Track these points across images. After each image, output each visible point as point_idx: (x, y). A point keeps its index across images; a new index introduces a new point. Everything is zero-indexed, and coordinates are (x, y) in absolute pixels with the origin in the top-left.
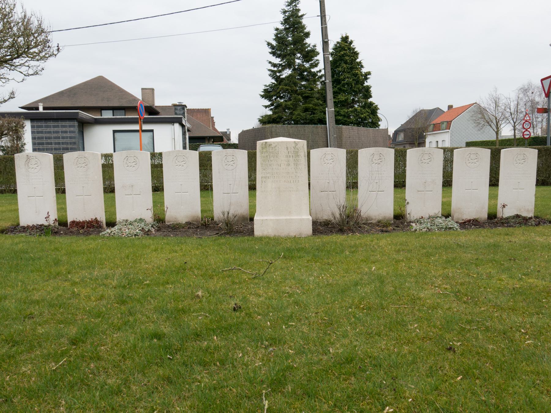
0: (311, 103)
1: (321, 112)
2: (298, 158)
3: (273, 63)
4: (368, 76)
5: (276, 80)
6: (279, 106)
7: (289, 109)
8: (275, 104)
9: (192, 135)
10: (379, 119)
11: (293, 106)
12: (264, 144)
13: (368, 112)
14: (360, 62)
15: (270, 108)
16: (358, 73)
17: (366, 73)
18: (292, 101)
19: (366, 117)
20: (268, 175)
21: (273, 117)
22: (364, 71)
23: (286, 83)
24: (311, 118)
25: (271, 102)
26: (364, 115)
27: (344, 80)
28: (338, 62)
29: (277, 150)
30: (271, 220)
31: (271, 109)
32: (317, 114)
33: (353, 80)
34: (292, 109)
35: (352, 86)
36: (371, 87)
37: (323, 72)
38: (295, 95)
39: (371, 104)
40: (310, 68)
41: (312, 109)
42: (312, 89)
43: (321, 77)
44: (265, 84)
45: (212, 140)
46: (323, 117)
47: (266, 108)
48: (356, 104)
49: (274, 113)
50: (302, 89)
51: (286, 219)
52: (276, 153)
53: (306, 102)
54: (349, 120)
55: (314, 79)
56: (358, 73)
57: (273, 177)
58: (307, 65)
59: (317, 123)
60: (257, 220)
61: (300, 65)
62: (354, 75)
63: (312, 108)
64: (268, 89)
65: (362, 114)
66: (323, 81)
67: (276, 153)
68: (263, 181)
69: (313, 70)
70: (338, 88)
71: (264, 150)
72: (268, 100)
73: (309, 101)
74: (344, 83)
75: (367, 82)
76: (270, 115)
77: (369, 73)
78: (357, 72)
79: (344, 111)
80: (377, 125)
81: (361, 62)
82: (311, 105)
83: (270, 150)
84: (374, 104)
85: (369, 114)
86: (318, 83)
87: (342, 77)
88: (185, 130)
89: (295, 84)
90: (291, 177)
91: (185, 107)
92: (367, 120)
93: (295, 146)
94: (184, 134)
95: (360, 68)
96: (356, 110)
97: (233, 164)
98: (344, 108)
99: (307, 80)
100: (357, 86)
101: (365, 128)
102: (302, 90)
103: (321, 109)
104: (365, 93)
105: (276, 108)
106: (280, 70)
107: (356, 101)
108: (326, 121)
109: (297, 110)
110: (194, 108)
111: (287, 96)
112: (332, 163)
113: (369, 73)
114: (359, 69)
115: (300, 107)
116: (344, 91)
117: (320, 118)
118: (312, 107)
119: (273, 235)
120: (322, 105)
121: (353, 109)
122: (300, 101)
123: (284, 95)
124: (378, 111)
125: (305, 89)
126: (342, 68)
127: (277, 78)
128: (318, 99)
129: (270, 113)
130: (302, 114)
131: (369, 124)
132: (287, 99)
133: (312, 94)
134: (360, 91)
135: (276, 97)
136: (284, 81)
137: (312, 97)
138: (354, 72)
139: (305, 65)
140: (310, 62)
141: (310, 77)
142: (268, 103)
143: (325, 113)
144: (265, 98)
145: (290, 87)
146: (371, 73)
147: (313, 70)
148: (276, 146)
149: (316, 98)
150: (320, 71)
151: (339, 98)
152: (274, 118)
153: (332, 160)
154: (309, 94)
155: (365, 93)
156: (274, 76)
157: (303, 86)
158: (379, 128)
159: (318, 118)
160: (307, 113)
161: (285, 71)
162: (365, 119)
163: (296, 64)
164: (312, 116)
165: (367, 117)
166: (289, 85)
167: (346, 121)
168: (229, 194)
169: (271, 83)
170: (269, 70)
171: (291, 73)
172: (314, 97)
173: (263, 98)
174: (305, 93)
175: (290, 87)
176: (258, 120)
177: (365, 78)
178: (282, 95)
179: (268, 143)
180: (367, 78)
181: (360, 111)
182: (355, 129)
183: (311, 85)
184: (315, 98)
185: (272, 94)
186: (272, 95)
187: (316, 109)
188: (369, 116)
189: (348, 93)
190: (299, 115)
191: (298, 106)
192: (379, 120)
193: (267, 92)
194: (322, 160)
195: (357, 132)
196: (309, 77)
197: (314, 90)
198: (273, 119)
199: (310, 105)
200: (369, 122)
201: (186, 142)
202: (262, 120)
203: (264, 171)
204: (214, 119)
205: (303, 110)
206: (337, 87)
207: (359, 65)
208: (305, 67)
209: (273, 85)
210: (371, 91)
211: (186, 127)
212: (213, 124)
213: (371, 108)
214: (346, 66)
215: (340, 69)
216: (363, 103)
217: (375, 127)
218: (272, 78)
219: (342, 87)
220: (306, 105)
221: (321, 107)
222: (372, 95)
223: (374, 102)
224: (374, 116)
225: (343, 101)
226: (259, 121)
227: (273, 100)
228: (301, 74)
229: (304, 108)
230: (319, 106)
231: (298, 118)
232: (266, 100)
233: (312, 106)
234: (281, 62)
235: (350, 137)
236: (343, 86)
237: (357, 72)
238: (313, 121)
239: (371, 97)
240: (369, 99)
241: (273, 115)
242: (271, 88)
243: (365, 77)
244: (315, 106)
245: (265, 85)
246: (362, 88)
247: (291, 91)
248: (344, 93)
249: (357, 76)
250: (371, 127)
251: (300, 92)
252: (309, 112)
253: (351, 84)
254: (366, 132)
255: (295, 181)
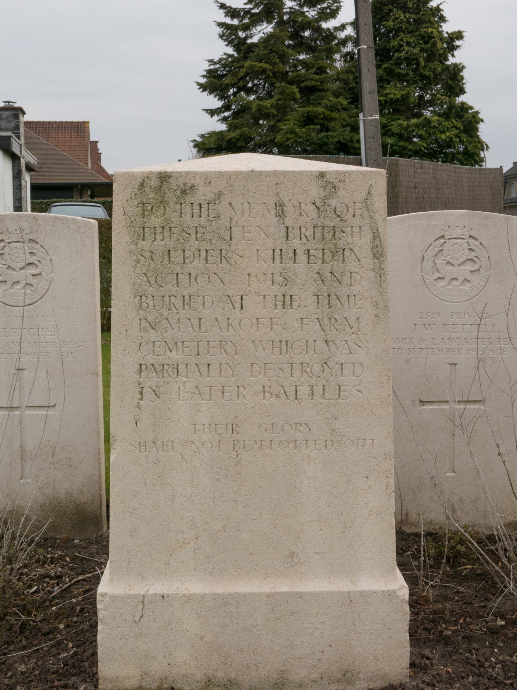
0: (321, 104)
1: (343, 126)
2: (338, 267)
3: (230, 7)
4: (457, 43)
5: (237, 49)
6: (243, 110)
7: (267, 116)
8: (233, 107)
9: (42, 180)
10: (482, 146)
11: (278, 110)
12: (154, 182)
13: (457, 128)
14: (438, 9)
15: (223, 115)
16: (432, 32)
17: (453, 33)
18: (276, 97)
19: (451, 139)
20: (175, 356)
21: (228, 137)
22: (447, 28)
23: (260, 54)
24: (320, 139)
25: (223, 102)
26: (448, 134)
27: (399, 49)
28: (386, 7)
29: (224, 221)
30: (189, 598)
31: (225, 119)
32: (335, 130)
33: (422, 50)
34: (274, 116)
35: (418, 64)
36: (463, 67)
37: (349, 31)
38: (283, 84)
39: (464, 108)
40: (318, 20)
41: (322, 119)
42: (321, 70)
43: (344, 42)
44: (210, 59)
45: (89, 193)
46: (348, 139)
47: (212, 116)
48: (426, 108)
49: (232, 127)
50: (298, 71)
51: (269, 596)
52: (221, 238)
53: (308, 101)
54: (410, 147)
55: (328, 46)
56: (432, 32)
57: (204, 369)
58: (311, 13)
59: (335, 152)
60: (114, 598)
61: (293, 13)
62: (422, 37)
63: (322, 116)
64: (216, 70)
65: (443, 132)
66: (348, 53)
67: (221, 238)
68: (146, 390)
69: (325, 25)
70: (385, 68)
71: (155, 221)
72: (217, 98)
73: (315, 100)
74: (400, 57)
75: (453, 56)
76: (221, 132)
77: (459, 35)
78: (430, 30)
79: (400, 125)
80: (476, 158)
81: (441, 7)
82: (320, 109)
83: (187, 218)
84: (471, 108)
85: (460, 133)
86: (337, 56)
87: (394, 43)
88: (20, 166)
89: (283, 58)
90: (297, 368)
91: (19, 112)
92: (454, 148)
93: (325, 198)
94: (17, 176)
95: (437, 21)
96: (428, 121)
97: (34, 281)
98: (398, 117)
99: (310, 49)
100: (431, 65)
101: (447, 166)
102: (299, 73)
103: (344, 120)
104: (450, 82)
105: (236, 115)
106: (245, 23)
107: (428, 101)
108: (359, 149)
109: (286, 121)
110: (53, 120)
111: (264, 87)
112: (469, 277)
113: (459, 35)
114: (436, 25)
115: (294, 113)
116: (401, 78)
117: (342, 141)
118: (323, 113)
119: (198, 676)
120: (345, 109)
121: (421, 119)
122: (295, 100)
123: (256, 84)
124: (481, 127)
125: (307, 70)
126: (394, 22)
127: (239, 43)
128: (337, 95)
129: (223, 127)
130: (298, 130)
131: (459, 157)
132: (262, 93)
133: (322, 82)
134: (436, 78)
135: (235, 90)
136: (257, 50)
137: (323, 90)
138: (423, 31)
139: (307, 14)
140: (319, 6)
141: (318, 42)
142: (215, 103)
143: (355, 129)
144: (211, 93)
145: (271, 64)
146: (464, 34)
147: (325, 25)
148: (220, 195)
149: (333, 93)
150: (343, 27)
151: (387, 94)
152: (231, 139)
153: (469, 267)
154: (316, 81)
155: (450, 82)
156: (233, 40)
157: (303, 63)
158: (481, 166)
159: (337, 139)
160: (312, 127)
161: (259, 28)
162: (450, 144)
163: (285, 10)
164: (323, 134)
165: (455, 139)
166: (268, 59)
167: (404, 148)
168: (17, 413)
169: (225, 54)
170: (221, 25)
171: (272, 30)
172: (328, 90)
173: (204, 90)
174: (306, 80)
175: (270, 65)
176: (192, 144)
177: (448, 48)
178: (250, 85)
179: (172, 181)
180: (453, 46)
181: (437, 125)
182: (429, 168)
183: (320, 62)
184: (329, 93)
185: (227, 82)
186: (228, 84)
187: (332, 119)
188: (459, 137)
189: (407, 81)
190: (292, 132)
191: (288, 110)
192: (481, 146)
193: (215, 77)
194: (428, 264)
195: (433, 173)
196: (315, 42)
197: (327, 73)
198: (229, 142)
199: (318, 109)
200: (459, 153)
201: (21, 197)
202: (203, 143)
203: (153, 335)
204: (99, 146)
205: (302, 119)
206: (383, 67)
207: (434, 15)
208: (306, 17)
209: (230, 60)
210: (462, 78)
211: (23, 161)
212: (96, 156)
213: (464, 119)
214: (405, 17)
215: (391, 23)
216: (445, 106)
217: (473, 163)
218: (226, 43)
219: (394, 67)
220: (310, 108)
221: (344, 115)
222: (467, 87)
223: (470, 103)
224: (471, 136)
225: (397, 100)
226: (195, 146)
227: (229, 96)
228: (296, 35)
229: (302, 116)
230: (339, 111)
231: (288, 139)
232: (212, 95)
233: (323, 110)
234: (249, 6)
235: (415, 188)
236: (398, 63)
237: (430, 30)
238: (325, 148)
239: (462, 91)
240: (458, 96)
241: (228, 131)
242: (224, 66)
243: (448, 43)
244: (331, 111)
245: (211, 61)
246: (443, 70)
247: (274, 73)
248: (399, 81)
249: (431, 41)
250: (463, 164)
251: (295, 77)
252: (316, 124)
253: (417, 59)
254: (453, 174)
255: (318, 390)
